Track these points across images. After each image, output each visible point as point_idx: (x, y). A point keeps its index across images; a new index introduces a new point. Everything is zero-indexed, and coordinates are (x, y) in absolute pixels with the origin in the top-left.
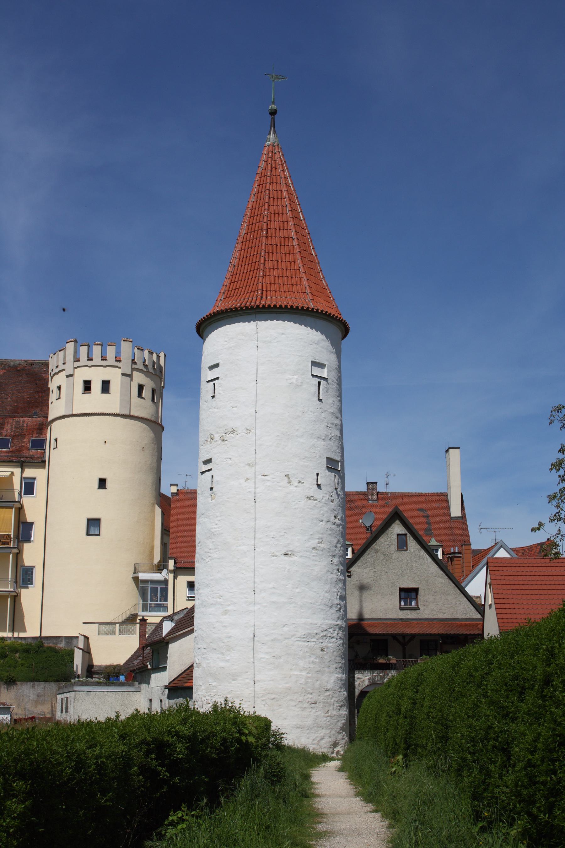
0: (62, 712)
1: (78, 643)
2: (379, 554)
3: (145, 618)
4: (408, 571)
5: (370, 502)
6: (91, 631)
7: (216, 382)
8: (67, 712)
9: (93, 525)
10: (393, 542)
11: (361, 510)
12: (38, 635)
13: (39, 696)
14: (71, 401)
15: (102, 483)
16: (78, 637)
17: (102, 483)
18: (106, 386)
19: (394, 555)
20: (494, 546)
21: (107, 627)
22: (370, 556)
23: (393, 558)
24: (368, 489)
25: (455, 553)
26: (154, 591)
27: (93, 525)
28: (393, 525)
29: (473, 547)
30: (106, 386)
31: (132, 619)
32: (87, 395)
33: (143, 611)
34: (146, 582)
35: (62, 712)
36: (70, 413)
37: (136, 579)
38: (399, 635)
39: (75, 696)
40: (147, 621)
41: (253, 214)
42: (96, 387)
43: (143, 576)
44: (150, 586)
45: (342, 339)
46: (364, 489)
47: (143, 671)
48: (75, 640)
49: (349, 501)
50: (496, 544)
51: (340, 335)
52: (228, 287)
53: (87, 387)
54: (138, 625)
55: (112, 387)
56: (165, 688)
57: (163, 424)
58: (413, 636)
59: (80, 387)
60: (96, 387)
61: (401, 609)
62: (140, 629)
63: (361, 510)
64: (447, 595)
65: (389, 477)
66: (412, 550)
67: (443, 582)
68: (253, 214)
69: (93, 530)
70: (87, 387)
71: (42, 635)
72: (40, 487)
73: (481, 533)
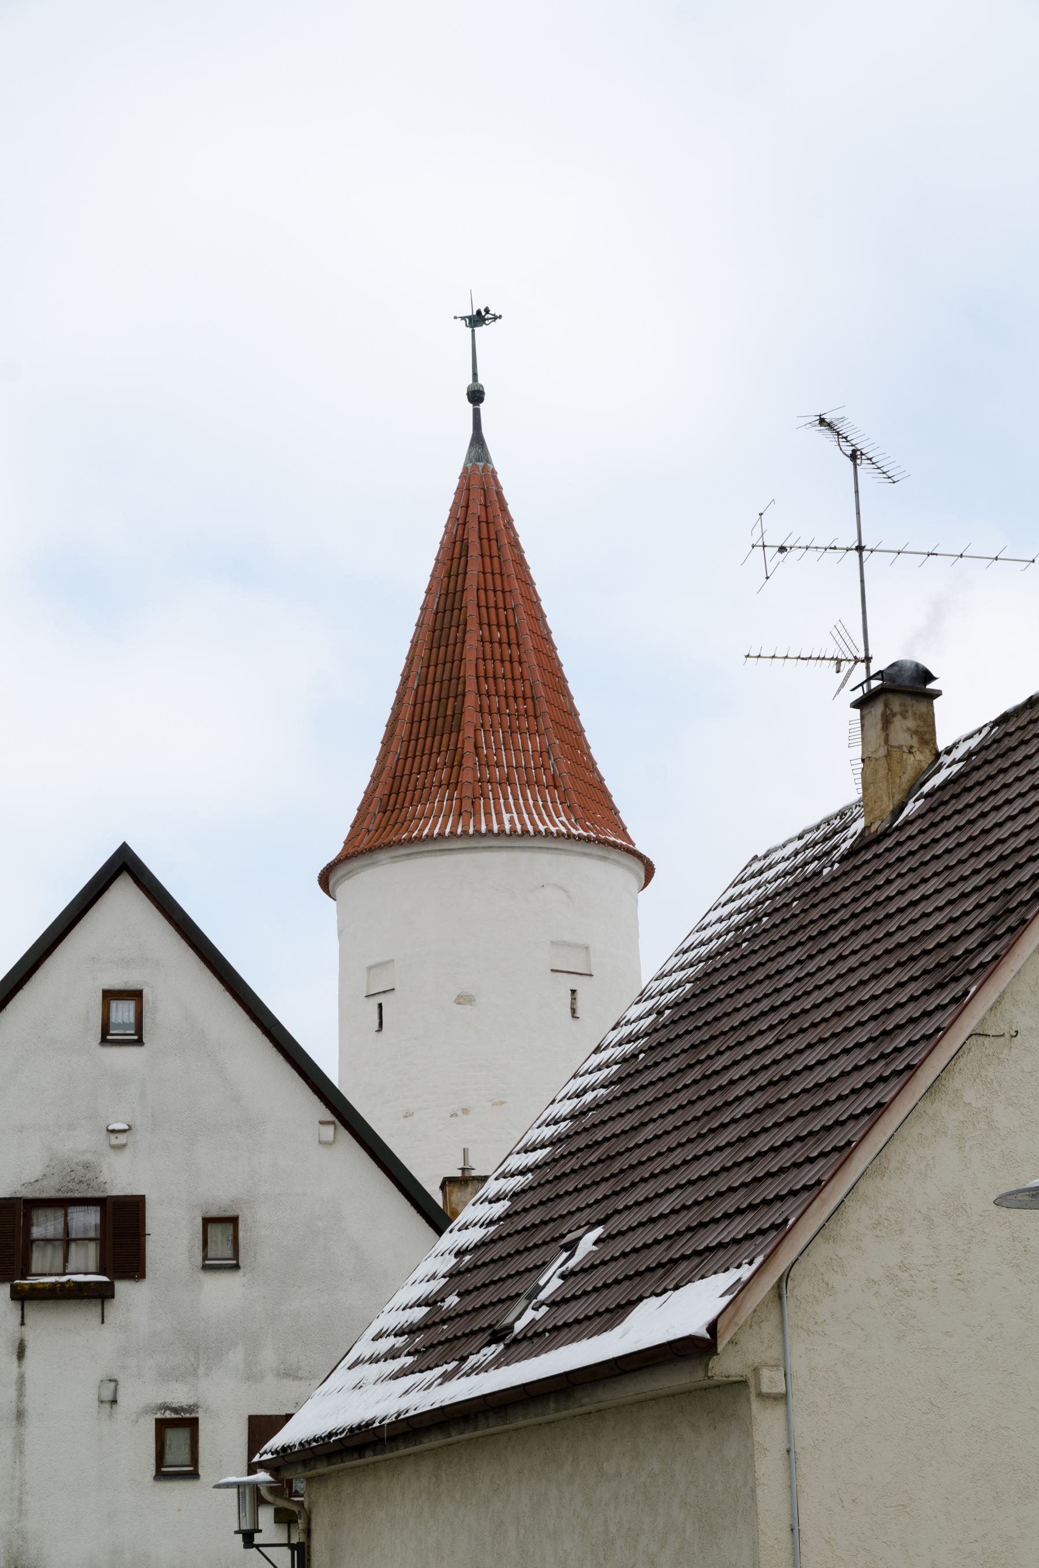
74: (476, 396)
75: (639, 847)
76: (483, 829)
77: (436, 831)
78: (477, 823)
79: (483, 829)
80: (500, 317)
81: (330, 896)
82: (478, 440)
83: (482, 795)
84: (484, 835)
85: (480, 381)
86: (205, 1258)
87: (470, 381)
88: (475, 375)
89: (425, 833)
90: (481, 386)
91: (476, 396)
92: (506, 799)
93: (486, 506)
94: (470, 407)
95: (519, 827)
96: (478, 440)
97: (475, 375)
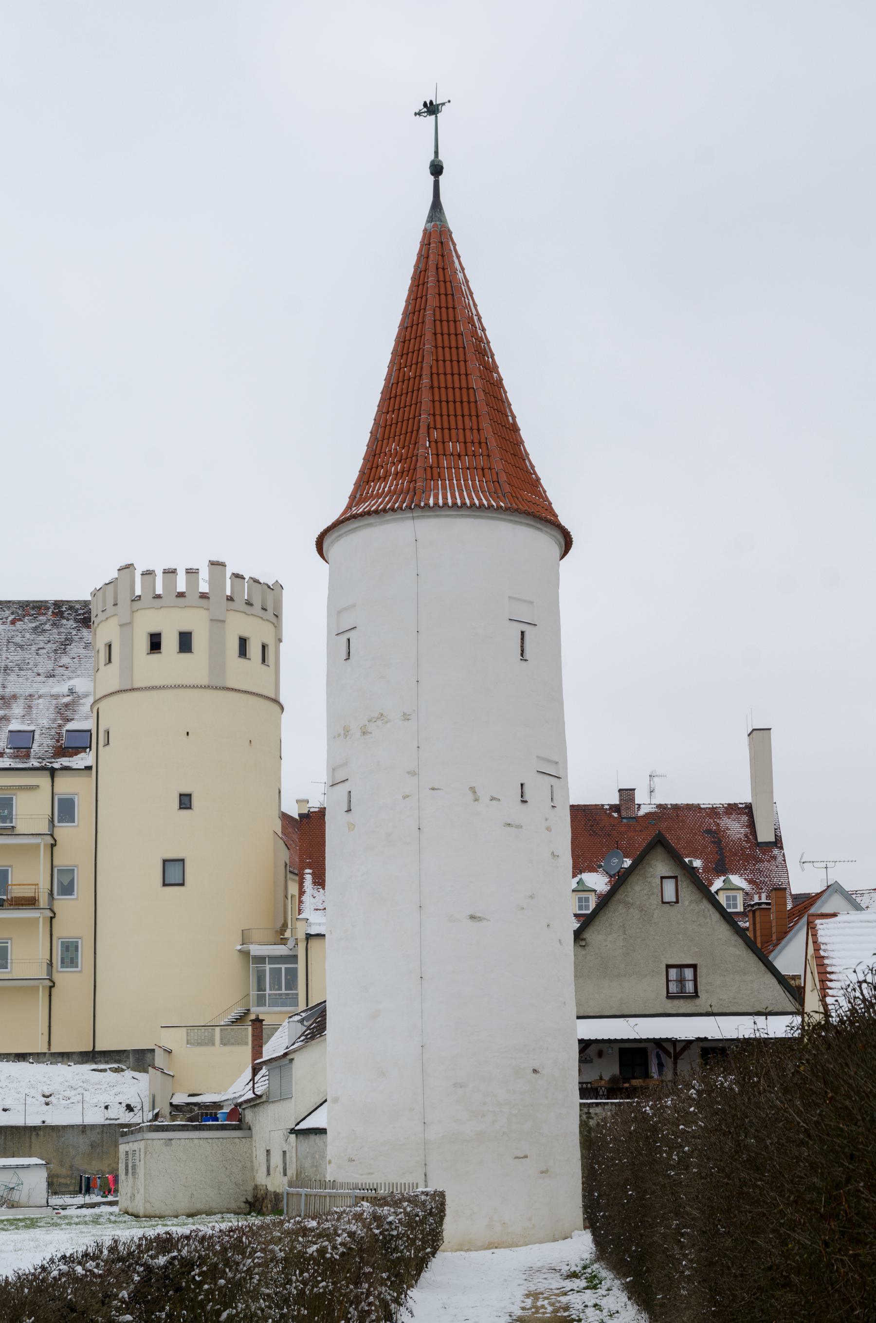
0: (127, 1174)
1: (154, 1059)
2: (631, 910)
3: (261, 1018)
4: (680, 936)
5: (624, 820)
6: (174, 1040)
7: (351, 635)
8: (134, 1174)
9: (173, 872)
10: (655, 890)
11: (609, 835)
12: (91, 1049)
13: (93, 1146)
14: (128, 668)
15: (185, 801)
16: (153, 1050)
17: (185, 801)
18: (185, 642)
19: (656, 912)
20: (824, 891)
21: (200, 1035)
22: (617, 914)
23: (655, 916)
24: (620, 800)
25: (760, 904)
26: (276, 973)
27: (173, 872)
28: (654, 862)
29: (795, 891)
30: (185, 642)
31: (239, 1020)
32: (155, 657)
33: (258, 1006)
34: (260, 959)
35: (127, 1174)
36: (129, 687)
37: (245, 954)
38: (667, 1040)
39: (146, 1148)
40: (264, 1023)
41: (406, 349)
42: (170, 643)
43: (256, 950)
44: (268, 967)
45: (562, 558)
46: (615, 800)
47: (255, 1106)
48: (149, 1056)
49: (589, 820)
50: (828, 887)
51: (557, 551)
52: (367, 475)
53: (155, 644)
54: (250, 1028)
55: (197, 642)
56: (291, 1133)
57: (282, 701)
58: (688, 1043)
59: (144, 643)
60: (170, 643)
61: (669, 997)
62: (253, 1036)
63: (609, 835)
64: (745, 974)
65: (655, 779)
66: (687, 903)
67: (738, 952)
68: (406, 349)
69: (174, 875)
70: (155, 644)
71: (97, 1049)
72: (83, 809)
73: (803, 869)
74: (437, 169)
75: (563, 521)
76: (441, 502)
77: (396, 505)
78: (436, 497)
79: (441, 502)
80: (416, 114)
81: (324, 558)
82: (436, 206)
83: (439, 477)
84: (423, 508)
85: (440, 158)
86: (668, 992)
87: (432, 157)
88: (436, 153)
89: (396, 505)
90: (440, 161)
91: (437, 169)
92: (451, 480)
93: (443, 256)
94: (432, 178)
95: (459, 502)
96: (436, 206)
97: (436, 153)
